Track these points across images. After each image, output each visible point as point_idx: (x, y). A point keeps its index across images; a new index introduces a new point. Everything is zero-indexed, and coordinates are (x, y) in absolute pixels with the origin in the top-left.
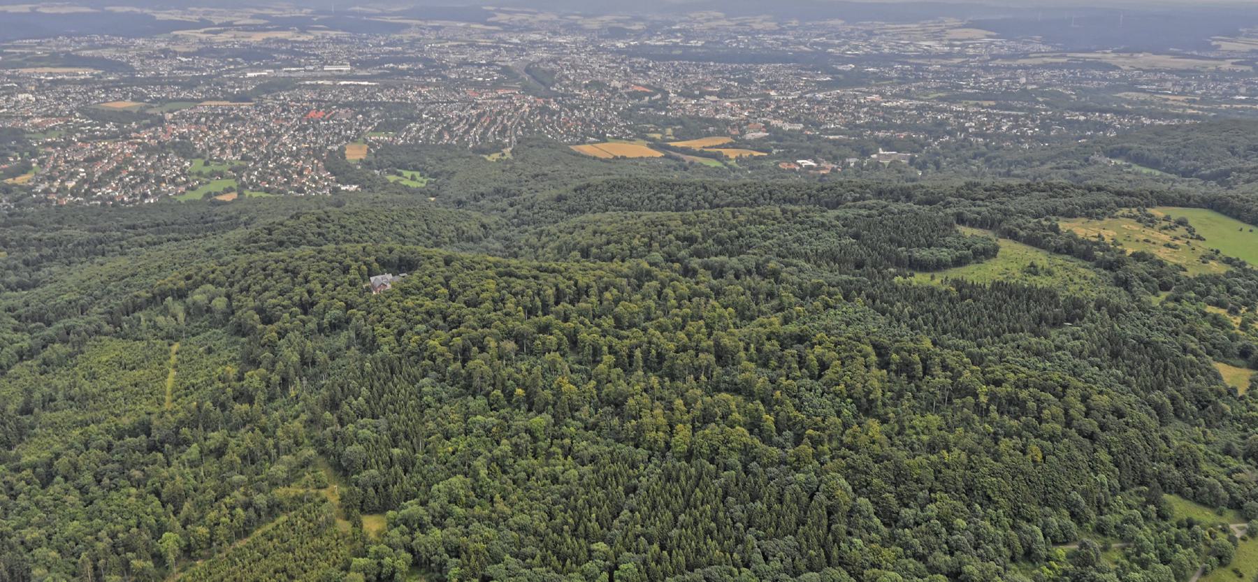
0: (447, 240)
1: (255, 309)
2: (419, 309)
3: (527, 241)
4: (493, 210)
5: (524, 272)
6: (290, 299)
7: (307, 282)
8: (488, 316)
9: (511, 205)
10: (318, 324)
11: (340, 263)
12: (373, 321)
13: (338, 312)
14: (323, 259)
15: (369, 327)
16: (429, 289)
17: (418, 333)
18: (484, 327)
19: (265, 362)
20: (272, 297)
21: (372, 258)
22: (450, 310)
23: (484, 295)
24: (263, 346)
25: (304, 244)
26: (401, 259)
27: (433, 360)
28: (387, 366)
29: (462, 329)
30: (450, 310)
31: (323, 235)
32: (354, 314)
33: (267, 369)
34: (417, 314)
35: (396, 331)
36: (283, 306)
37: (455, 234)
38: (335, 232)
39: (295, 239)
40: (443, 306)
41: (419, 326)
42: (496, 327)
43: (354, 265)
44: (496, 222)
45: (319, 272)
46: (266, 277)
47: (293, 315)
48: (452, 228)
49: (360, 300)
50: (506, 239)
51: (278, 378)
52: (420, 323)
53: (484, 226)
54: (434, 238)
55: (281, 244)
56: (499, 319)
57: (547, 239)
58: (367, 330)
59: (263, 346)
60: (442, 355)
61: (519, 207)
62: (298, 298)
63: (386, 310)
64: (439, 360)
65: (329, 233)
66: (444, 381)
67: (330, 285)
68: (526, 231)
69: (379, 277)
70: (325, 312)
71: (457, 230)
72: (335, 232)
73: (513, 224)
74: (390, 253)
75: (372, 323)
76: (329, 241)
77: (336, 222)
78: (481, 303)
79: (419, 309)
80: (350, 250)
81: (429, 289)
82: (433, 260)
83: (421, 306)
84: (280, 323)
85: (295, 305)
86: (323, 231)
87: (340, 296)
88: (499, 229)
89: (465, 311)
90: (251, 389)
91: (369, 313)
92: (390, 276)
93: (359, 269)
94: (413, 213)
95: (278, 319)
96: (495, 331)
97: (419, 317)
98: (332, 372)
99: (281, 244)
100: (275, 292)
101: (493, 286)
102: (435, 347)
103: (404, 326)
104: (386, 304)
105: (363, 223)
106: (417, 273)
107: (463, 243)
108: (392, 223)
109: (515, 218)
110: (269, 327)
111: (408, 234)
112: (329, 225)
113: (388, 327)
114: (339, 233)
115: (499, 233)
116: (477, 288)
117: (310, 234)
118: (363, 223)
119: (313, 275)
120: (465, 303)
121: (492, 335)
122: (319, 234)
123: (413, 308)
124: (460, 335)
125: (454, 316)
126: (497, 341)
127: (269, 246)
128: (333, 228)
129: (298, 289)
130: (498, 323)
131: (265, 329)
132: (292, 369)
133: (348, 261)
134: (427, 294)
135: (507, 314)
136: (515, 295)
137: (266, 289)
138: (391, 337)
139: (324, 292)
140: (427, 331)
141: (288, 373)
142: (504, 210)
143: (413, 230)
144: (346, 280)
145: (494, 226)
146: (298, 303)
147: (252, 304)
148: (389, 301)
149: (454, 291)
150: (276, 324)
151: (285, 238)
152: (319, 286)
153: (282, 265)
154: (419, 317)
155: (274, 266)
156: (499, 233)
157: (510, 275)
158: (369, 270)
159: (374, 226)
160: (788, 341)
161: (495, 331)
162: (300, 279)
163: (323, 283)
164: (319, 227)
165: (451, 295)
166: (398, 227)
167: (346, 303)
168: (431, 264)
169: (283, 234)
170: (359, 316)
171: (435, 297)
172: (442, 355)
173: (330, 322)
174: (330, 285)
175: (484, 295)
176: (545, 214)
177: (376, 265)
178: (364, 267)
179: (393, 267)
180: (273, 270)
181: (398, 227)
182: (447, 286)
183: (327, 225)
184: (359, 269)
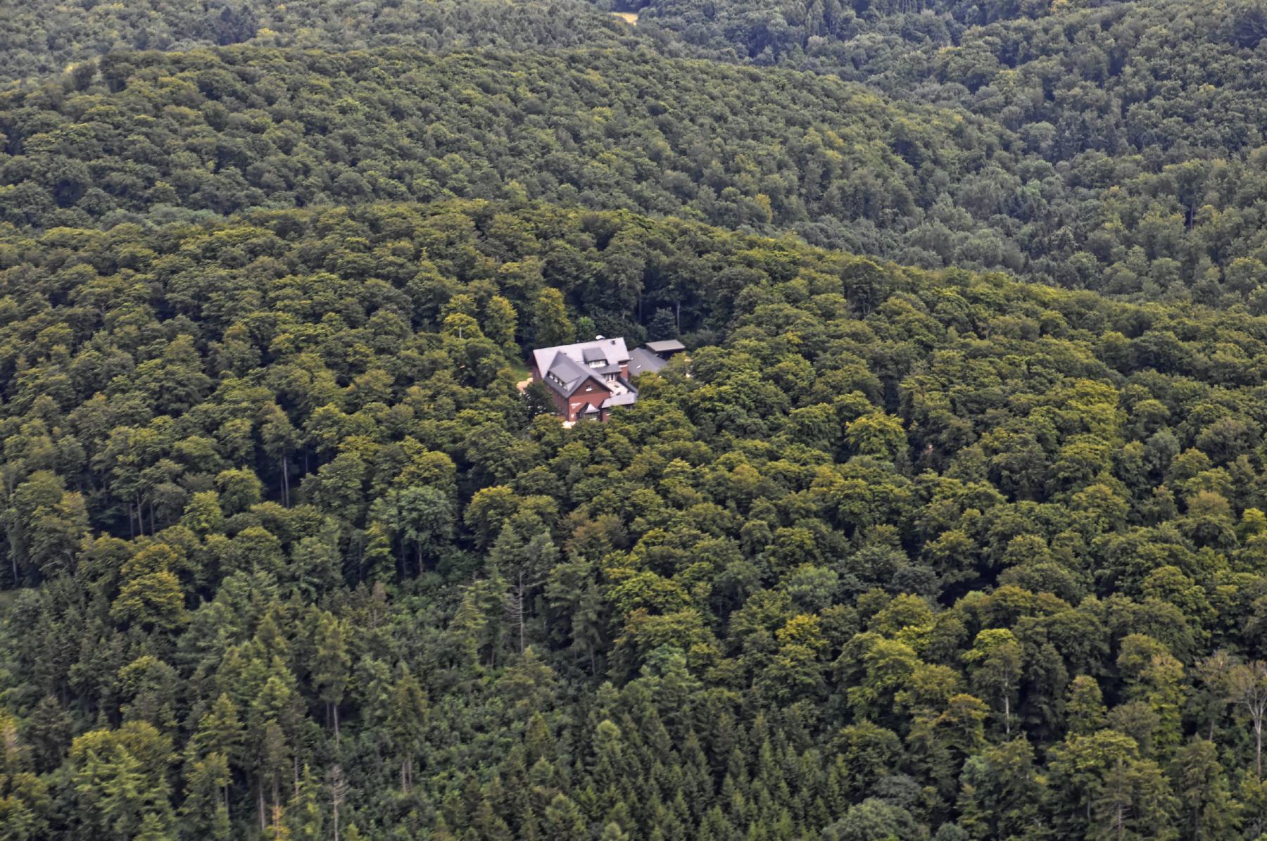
0: (763, 201)
1: (58, 465)
2: (796, 499)
3: (1130, 221)
4: (923, 75)
5: (1226, 354)
6: (210, 428)
7: (268, 358)
8: (1116, 540)
9: (1008, 57)
10: (345, 546)
11: (399, 282)
12: (593, 542)
13: (429, 492)
14: (316, 261)
15: (582, 566)
16: (817, 411)
17: (804, 603)
18: (1105, 588)
19: (147, 697)
20: (131, 419)
21: (531, 266)
22: (936, 508)
23: (1078, 447)
24: (124, 627)
25: (163, 197)
26: (652, 277)
27: (895, 719)
28: (692, 741)
29: (1010, 590)
30: (936, 508)
31: (242, 162)
32: (506, 510)
33: (159, 723)
34: (786, 517)
35: (702, 588)
36: (181, 458)
37: (792, 175)
38: (286, 147)
39: (125, 173)
40: (898, 487)
41: (809, 570)
42: (1167, 592)
43: (461, 296)
44: (957, 133)
45: (315, 316)
46: (84, 330)
47: (236, 504)
48: (777, 149)
49: (523, 446)
50: (1019, 210)
51: (218, 761)
52: (809, 556)
53: (903, 146)
54: (706, 191)
55: (66, 192)
56: (1174, 559)
57: (1233, 214)
58: (567, 579)
59: (124, 627)
60: (938, 703)
61: (1052, 64)
62: (246, 425)
63: (643, 493)
64: (924, 722)
65: (263, 151)
66: (954, 816)
67: (377, 376)
68: (1106, 177)
69: (574, 351)
70: (367, 495)
71: (801, 158)
72: (286, 147)
73: (1032, 146)
74: (602, 244)
75: (591, 549)
76: (270, 189)
77: (283, 105)
78: (1066, 484)
79: (796, 499)
80: (429, 228)
81: (817, 411)
82: (797, 283)
83: (800, 484)
84: (183, 531)
85: (232, 456)
86: (239, 142)
87: (428, 425)
88: (975, 166)
89: (1005, 513)
90: (108, 807)
91: (568, 505)
92: (615, 350)
93: (481, 312)
94: (594, 77)
95: (177, 511)
96: (1168, 609)
97: (800, 534)
98: (433, 756)
99: (66, 192)
100: (136, 401)
101: (1109, 410)
102: (899, 666)
103: (738, 566)
104: (637, 467)
105: (398, 114)
106: (748, 338)
107: (830, 222)
108: (517, 119)
109: (1034, 115)
110: (144, 547)
111: (593, 168)
112: (261, 116)
113: (666, 568)
114: (302, 153)
115: (973, 184)
116: (1036, 416)
117: (184, 156)
118: (398, 114)
119: (287, 331)
120: (995, 476)
121: (1150, 622)
122: (223, 157)
123: (763, 491)
124: (1005, 617)
125: (954, 535)
126: (1187, 654)
127: (20, 200)
128: (275, 132)
129: (235, 389)
130: (1167, 571)
131: (517, 567)
132: (272, 728)
133: (429, 273)
134: (805, 434)
135: (1201, 538)
136: (1220, 452)
137: (89, 385)
138: (689, 613)
139: (352, 408)
140: (847, 596)
141: (257, 746)
142: (976, 82)
143: (614, 153)
144: (440, 354)
145: (950, 152)
146: (246, 447)
147: (43, 446)
148: (650, 453)
149: (931, 425)
150: (170, 533)
151: (78, 168)
152: (327, 379)
153: (141, 284)
154: (800, 534)
155: (100, 285)
156: (973, 184)
157: (1164, 362)
158: (524, 319)
159: (443, 129)
160: (397, 672)
161: (1168, 609)
162: (236, 346)
163: (347, 370)
164: (217, 123)
165: (916, 445)
166: (546, 136)
167: (457, 456)
168: (793, 299)
169: (71, 148)
170: (526, 514)
171: (843, 452)
172: (938, 703)
173: (396, 538)
174: (377, 376)
175: (1078, 447)
176: (1182, 101)
177: (550, 297)
178: (504, 304)
179: (618, 306)
180: (103, 302)
181: (546, 136)
182: (891, 400)
183: (246, 116)
184: (481, 312)
